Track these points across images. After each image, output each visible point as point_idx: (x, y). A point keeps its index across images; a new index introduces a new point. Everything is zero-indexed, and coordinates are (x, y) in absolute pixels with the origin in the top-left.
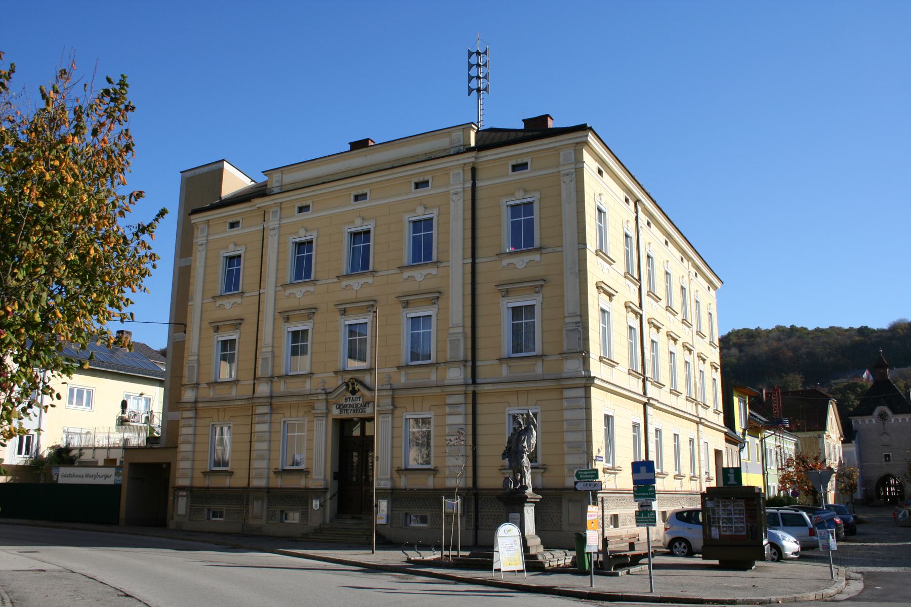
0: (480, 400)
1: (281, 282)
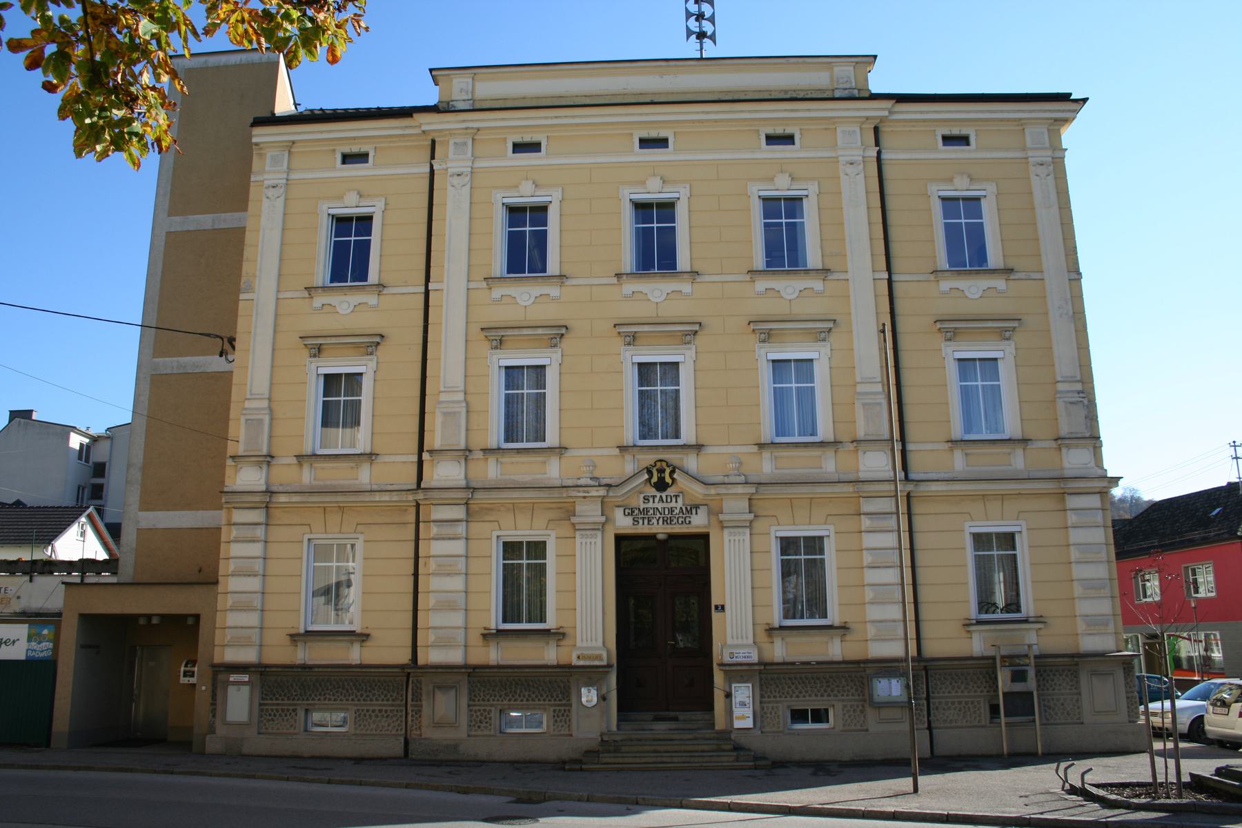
0: (917, 508)
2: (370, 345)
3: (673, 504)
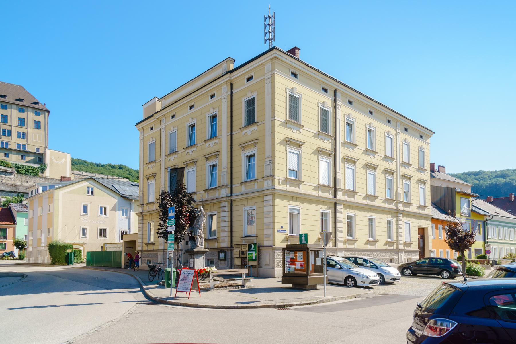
1: (145, 163)
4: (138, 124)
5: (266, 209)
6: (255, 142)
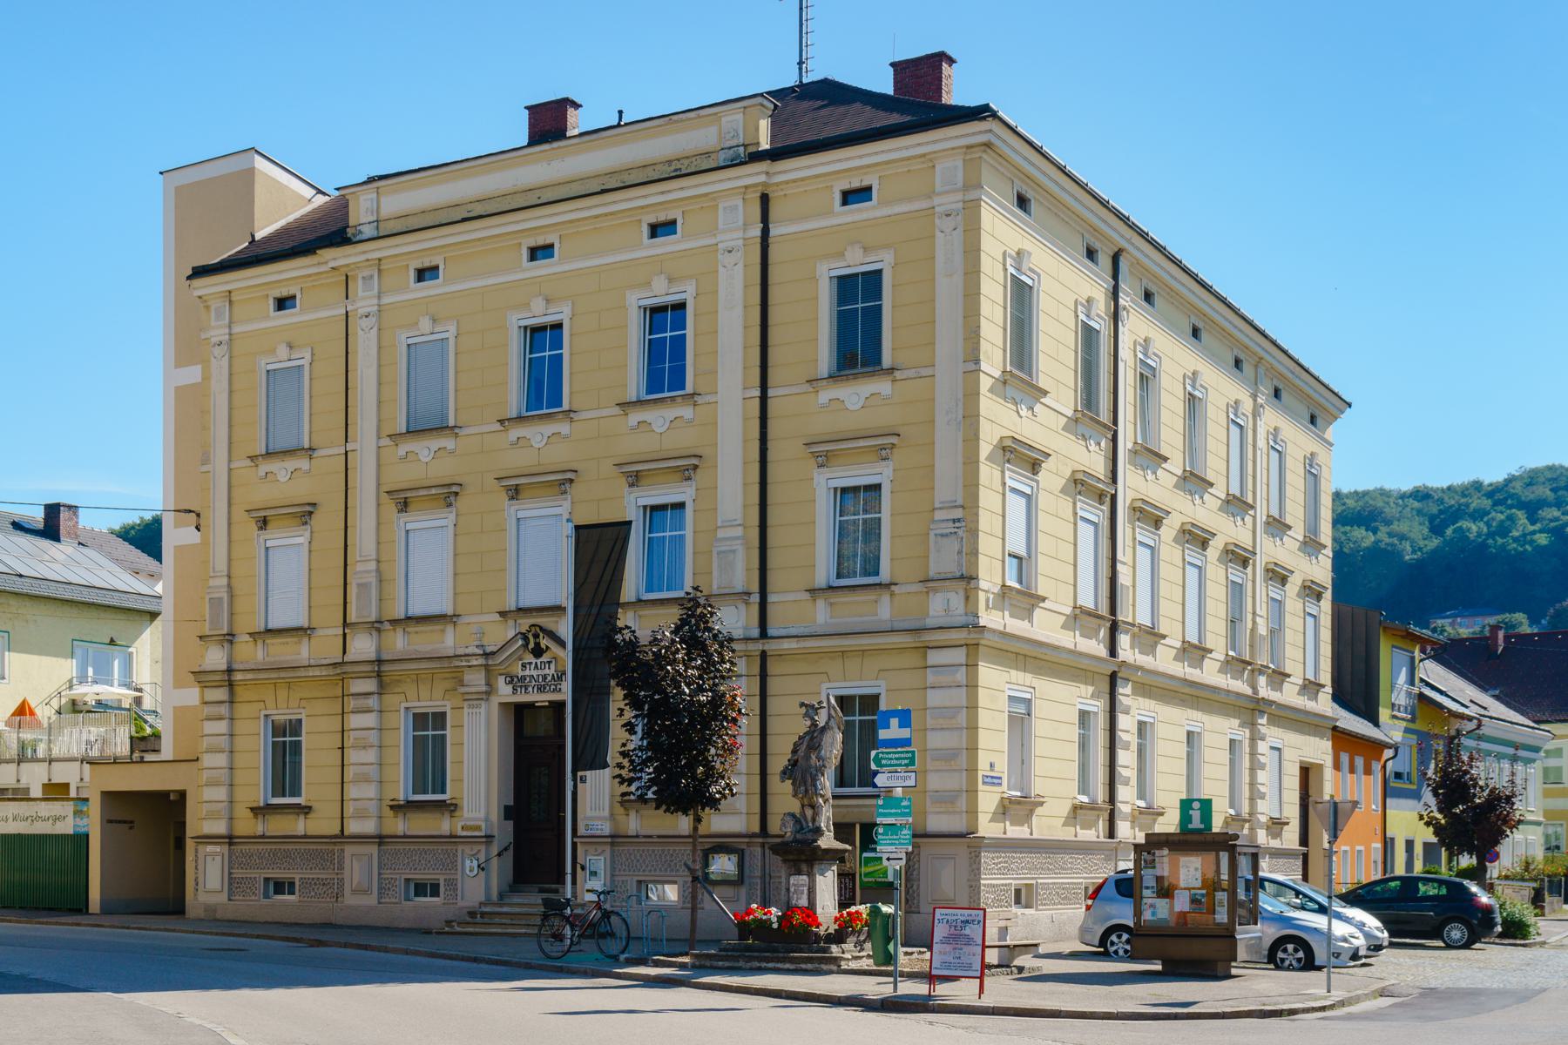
0: (773, 668)
2: (562, 483)
3: (547, 671)
4: (200, 272)
5: (935, 698)
6: (883, 443)
